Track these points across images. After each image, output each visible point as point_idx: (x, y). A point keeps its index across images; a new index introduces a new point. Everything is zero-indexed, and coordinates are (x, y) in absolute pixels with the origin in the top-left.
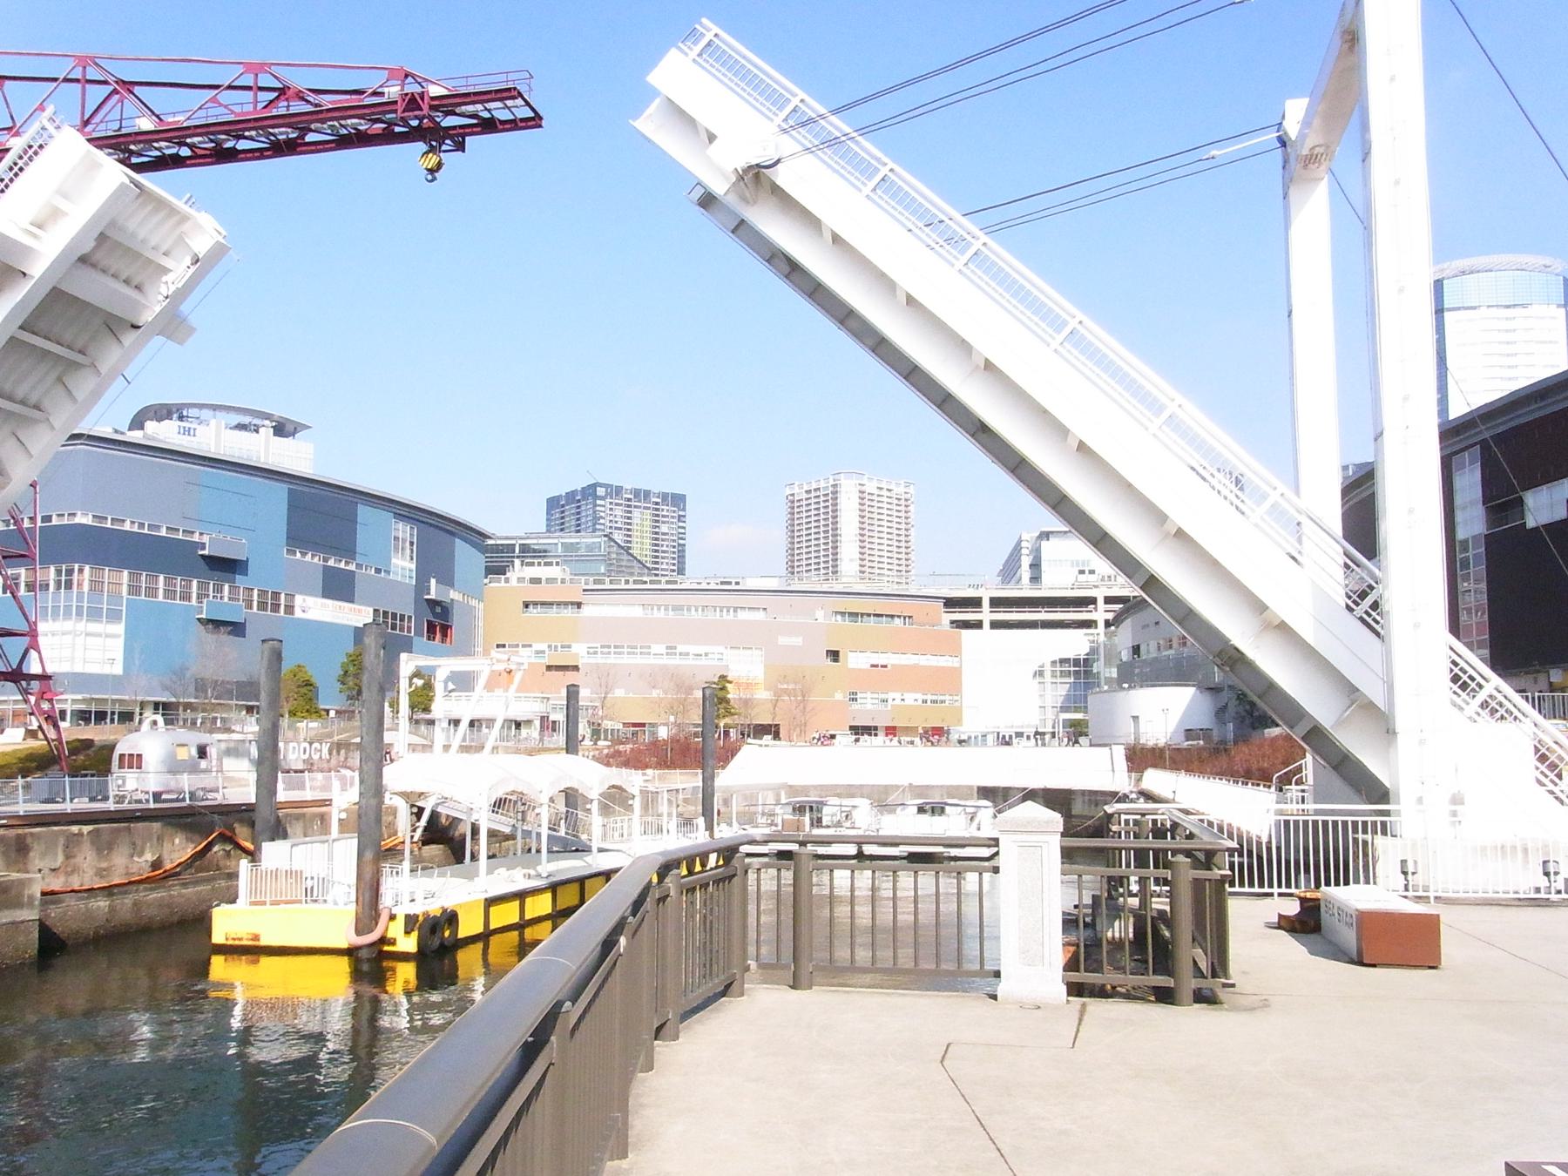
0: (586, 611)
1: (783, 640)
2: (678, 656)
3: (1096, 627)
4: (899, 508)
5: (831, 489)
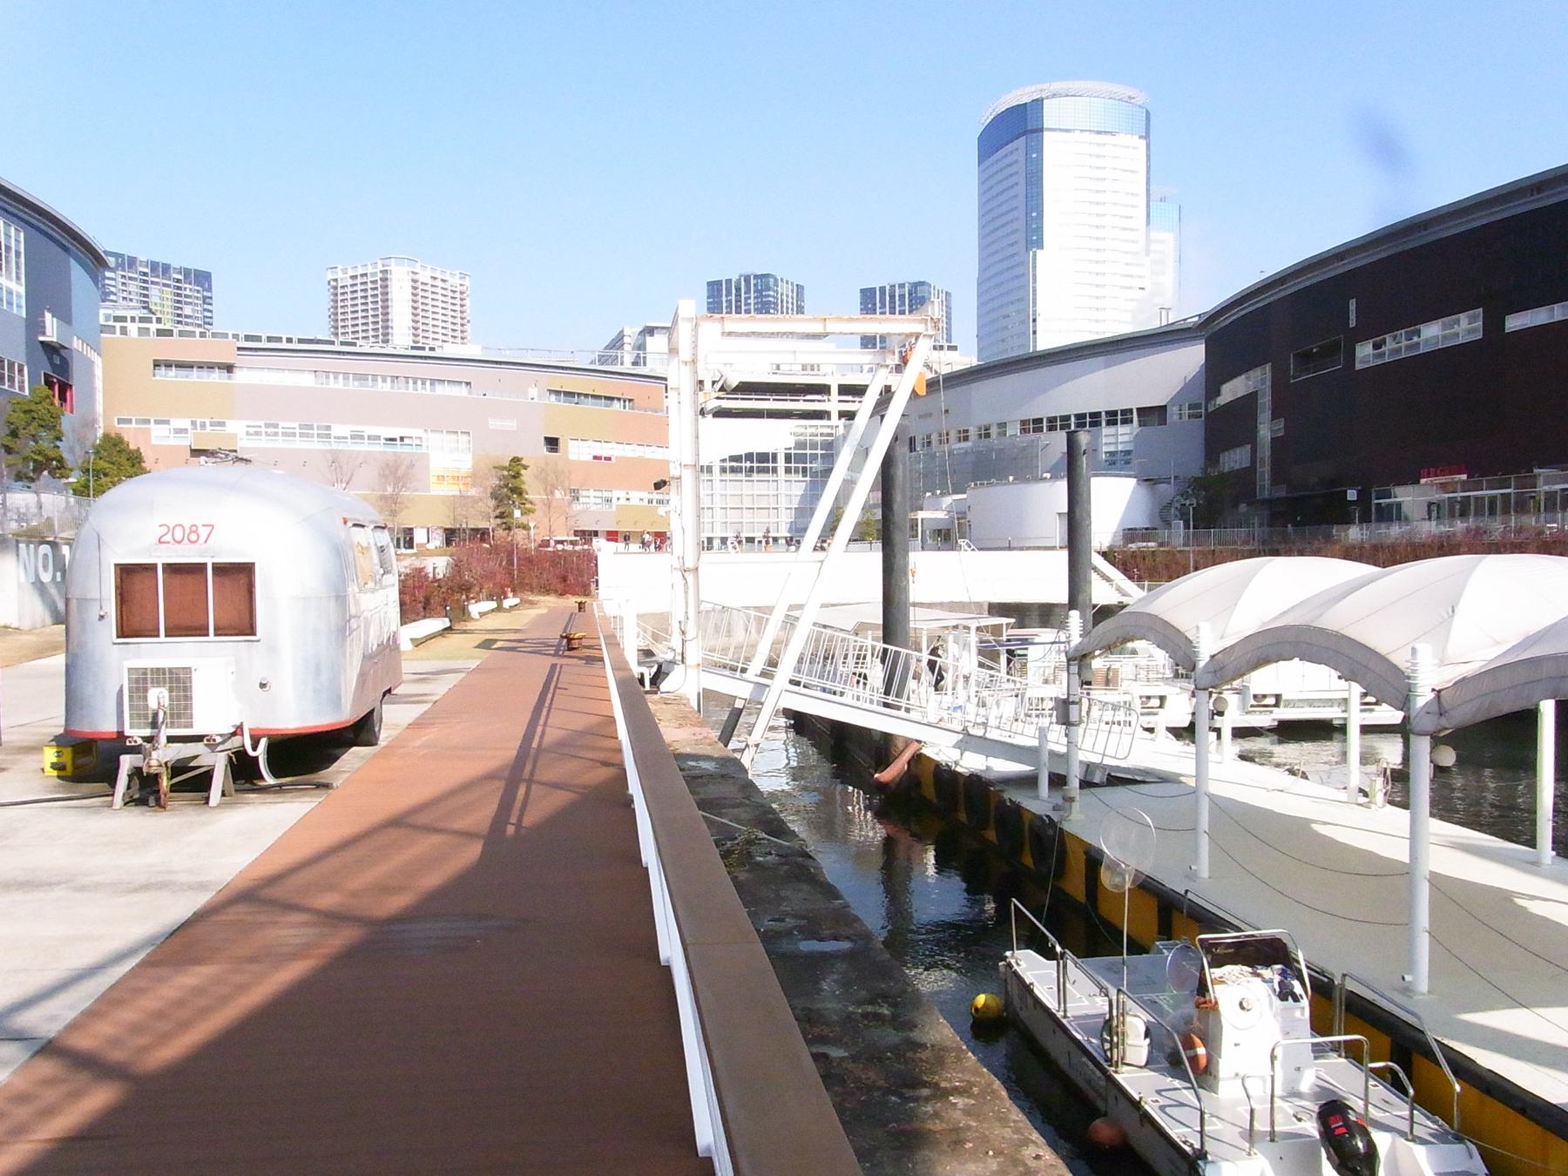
0: (240, 376)
1: (494, 424)
2: (366, 441)
3: (829, 418)
4: (453, 301)
5: (380, 275)
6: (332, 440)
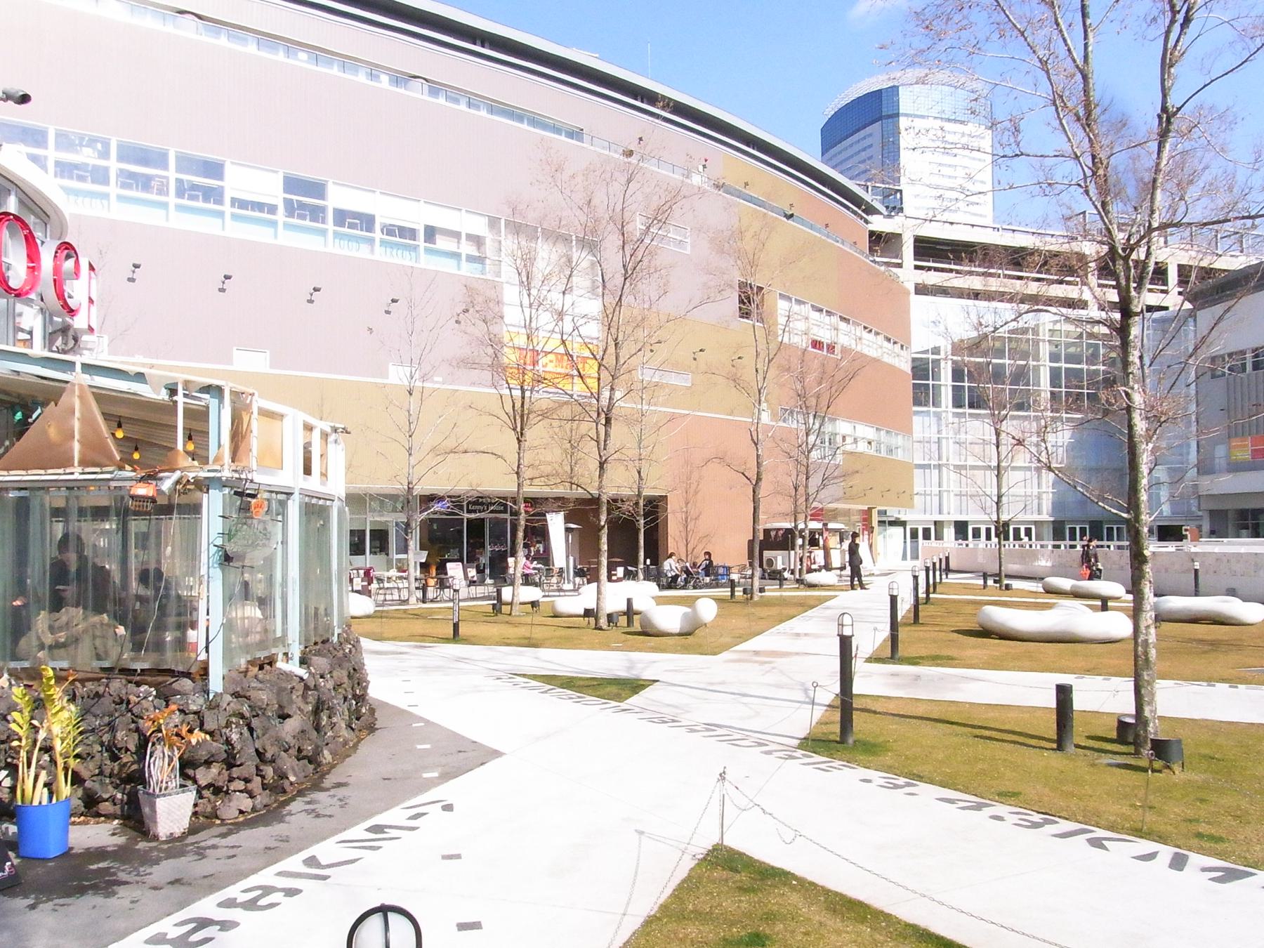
6: (227, 208)
